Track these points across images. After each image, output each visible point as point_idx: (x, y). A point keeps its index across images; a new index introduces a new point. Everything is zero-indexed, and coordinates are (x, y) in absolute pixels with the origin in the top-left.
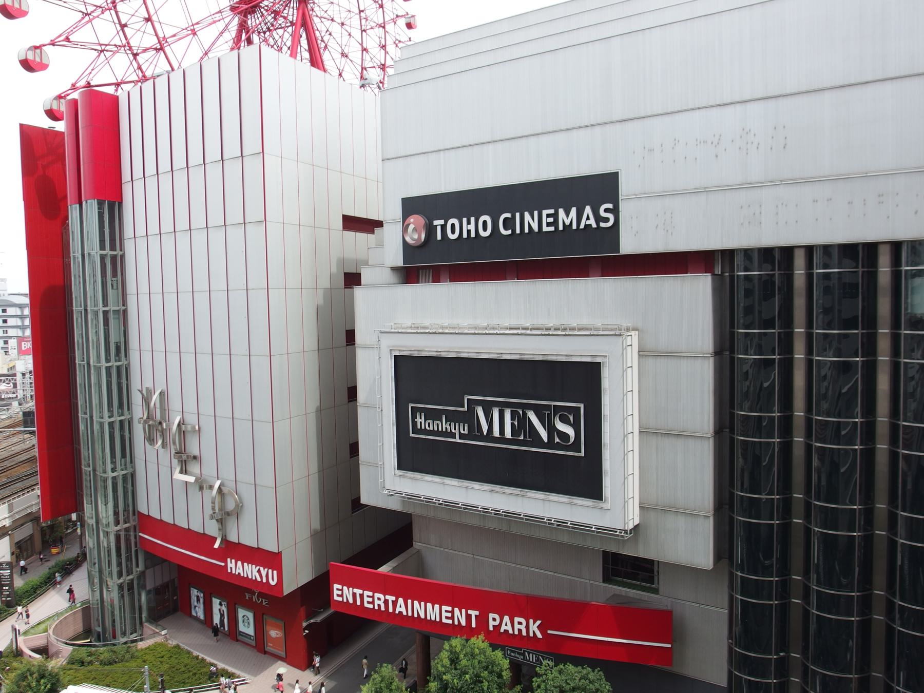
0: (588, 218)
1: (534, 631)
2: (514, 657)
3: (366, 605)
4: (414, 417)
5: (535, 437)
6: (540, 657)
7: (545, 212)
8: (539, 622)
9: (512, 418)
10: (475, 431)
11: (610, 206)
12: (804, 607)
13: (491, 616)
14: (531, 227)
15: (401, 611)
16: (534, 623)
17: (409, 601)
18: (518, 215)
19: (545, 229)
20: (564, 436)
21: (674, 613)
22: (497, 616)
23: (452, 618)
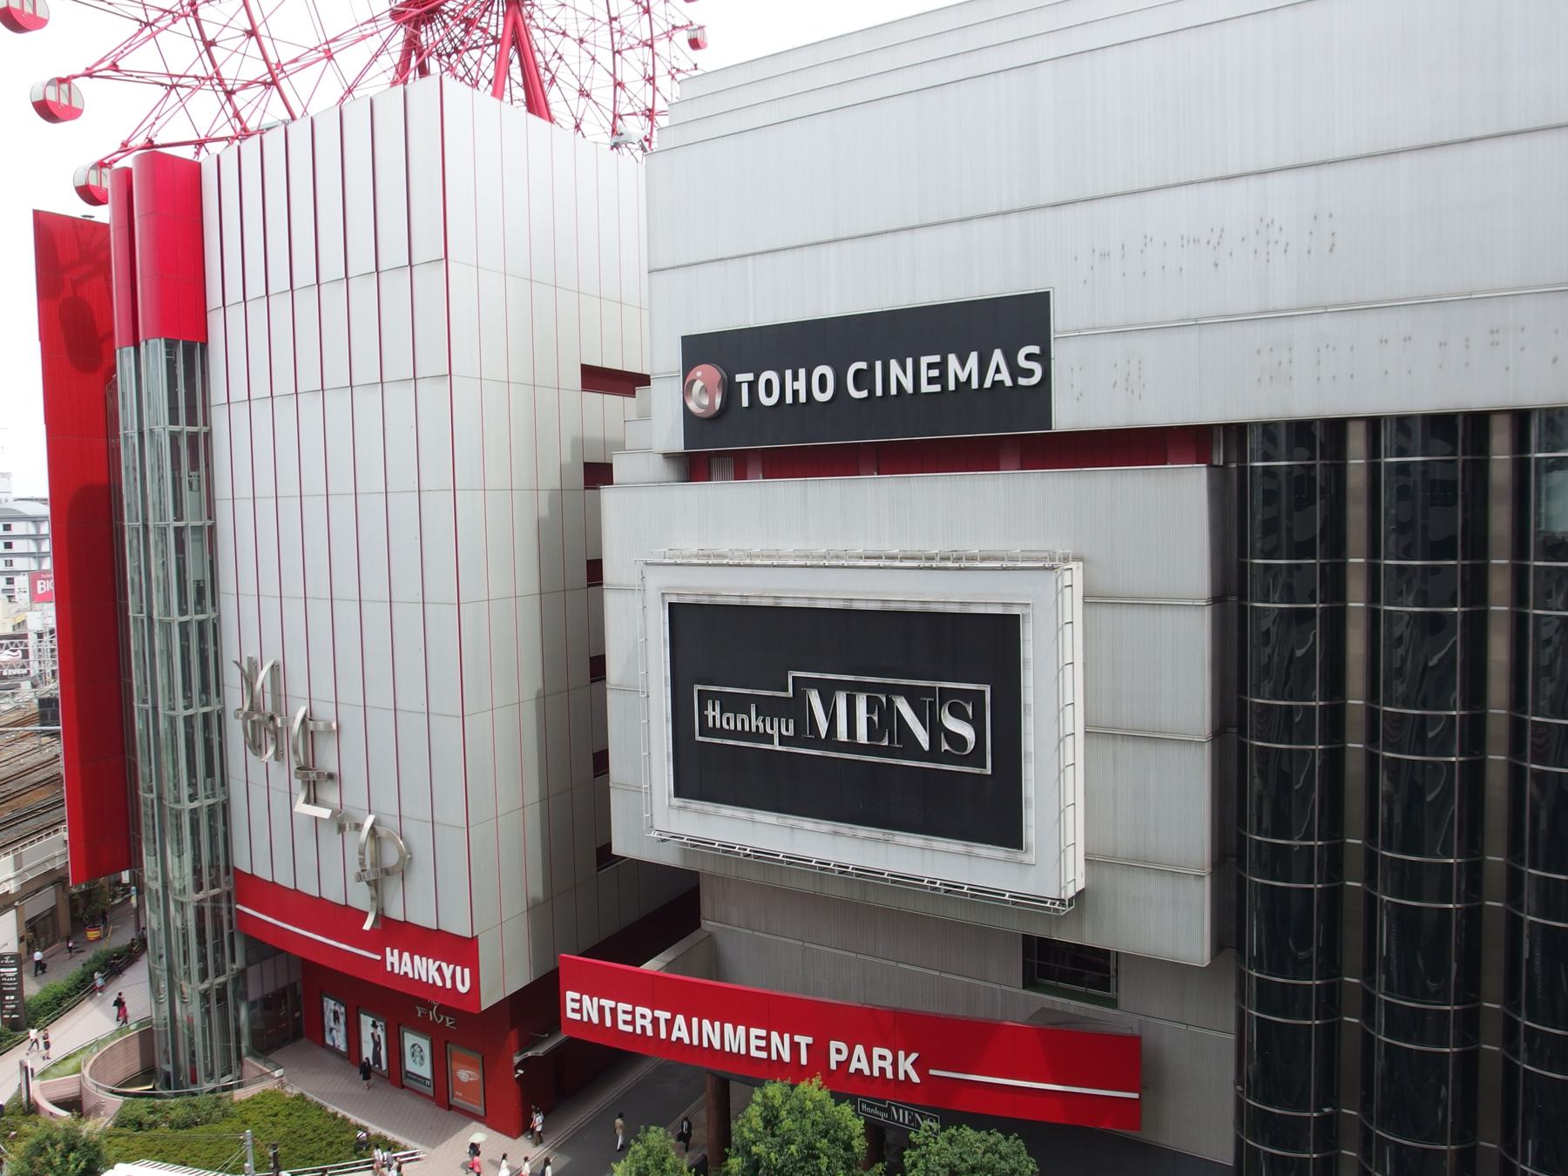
2: (872, 1114)
3: (622, 1027)
4: (703, 707)
5: (908, 742)
6: (917, 1115)
9: (870, 710)
20: (957, 740)
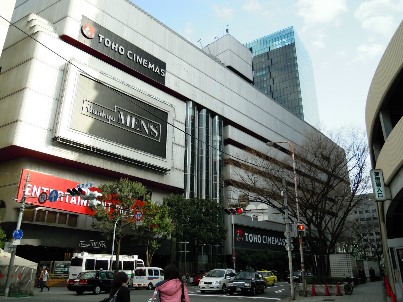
0: (157, 70)
4: (81, 243)
5: (100, 246)
6: (143, 122)
7: (144, 60)
9: (136, 121)
20: (103, 246)
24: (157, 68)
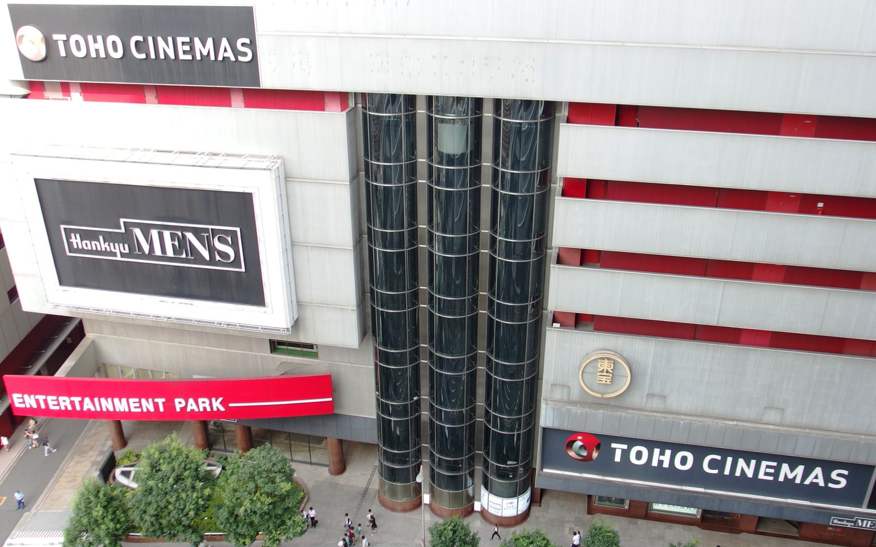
0: (225, 50)
1: (168, 46)
2: (97, 252)
4: (68, 238)
7: (180, 40)
8: (220, 399)
9: (173, 239)
10: (135, 249)
11: (247, 41)
12: (429, 311)
13: (177, 400)
14: (166, 52)
15: (89, 408)
16: (216, 400)
17: (96, 400)
18: (150, 39)
19: (182, 57)
21: (332, 376)
22: (181, 400)
23: (141, 406)
24: (224, 43)
